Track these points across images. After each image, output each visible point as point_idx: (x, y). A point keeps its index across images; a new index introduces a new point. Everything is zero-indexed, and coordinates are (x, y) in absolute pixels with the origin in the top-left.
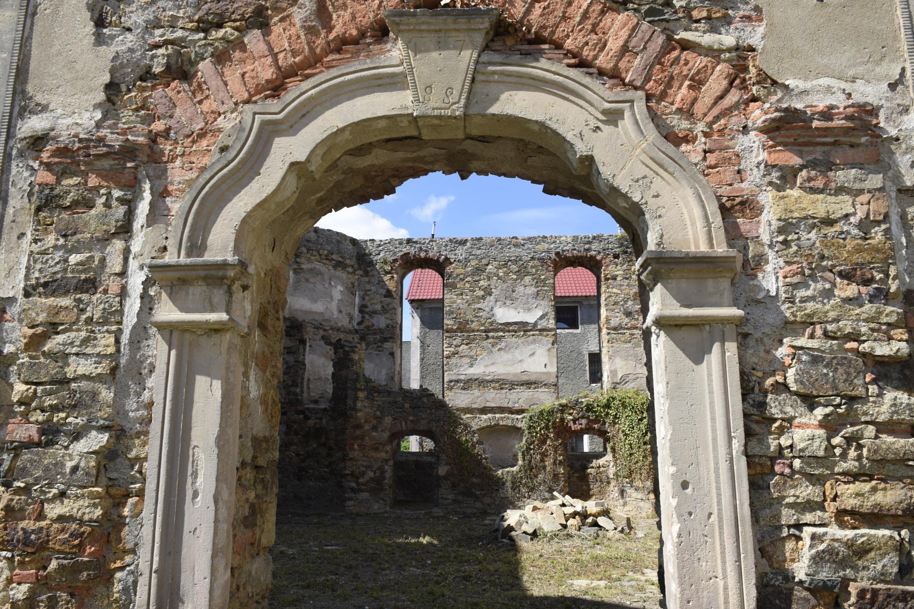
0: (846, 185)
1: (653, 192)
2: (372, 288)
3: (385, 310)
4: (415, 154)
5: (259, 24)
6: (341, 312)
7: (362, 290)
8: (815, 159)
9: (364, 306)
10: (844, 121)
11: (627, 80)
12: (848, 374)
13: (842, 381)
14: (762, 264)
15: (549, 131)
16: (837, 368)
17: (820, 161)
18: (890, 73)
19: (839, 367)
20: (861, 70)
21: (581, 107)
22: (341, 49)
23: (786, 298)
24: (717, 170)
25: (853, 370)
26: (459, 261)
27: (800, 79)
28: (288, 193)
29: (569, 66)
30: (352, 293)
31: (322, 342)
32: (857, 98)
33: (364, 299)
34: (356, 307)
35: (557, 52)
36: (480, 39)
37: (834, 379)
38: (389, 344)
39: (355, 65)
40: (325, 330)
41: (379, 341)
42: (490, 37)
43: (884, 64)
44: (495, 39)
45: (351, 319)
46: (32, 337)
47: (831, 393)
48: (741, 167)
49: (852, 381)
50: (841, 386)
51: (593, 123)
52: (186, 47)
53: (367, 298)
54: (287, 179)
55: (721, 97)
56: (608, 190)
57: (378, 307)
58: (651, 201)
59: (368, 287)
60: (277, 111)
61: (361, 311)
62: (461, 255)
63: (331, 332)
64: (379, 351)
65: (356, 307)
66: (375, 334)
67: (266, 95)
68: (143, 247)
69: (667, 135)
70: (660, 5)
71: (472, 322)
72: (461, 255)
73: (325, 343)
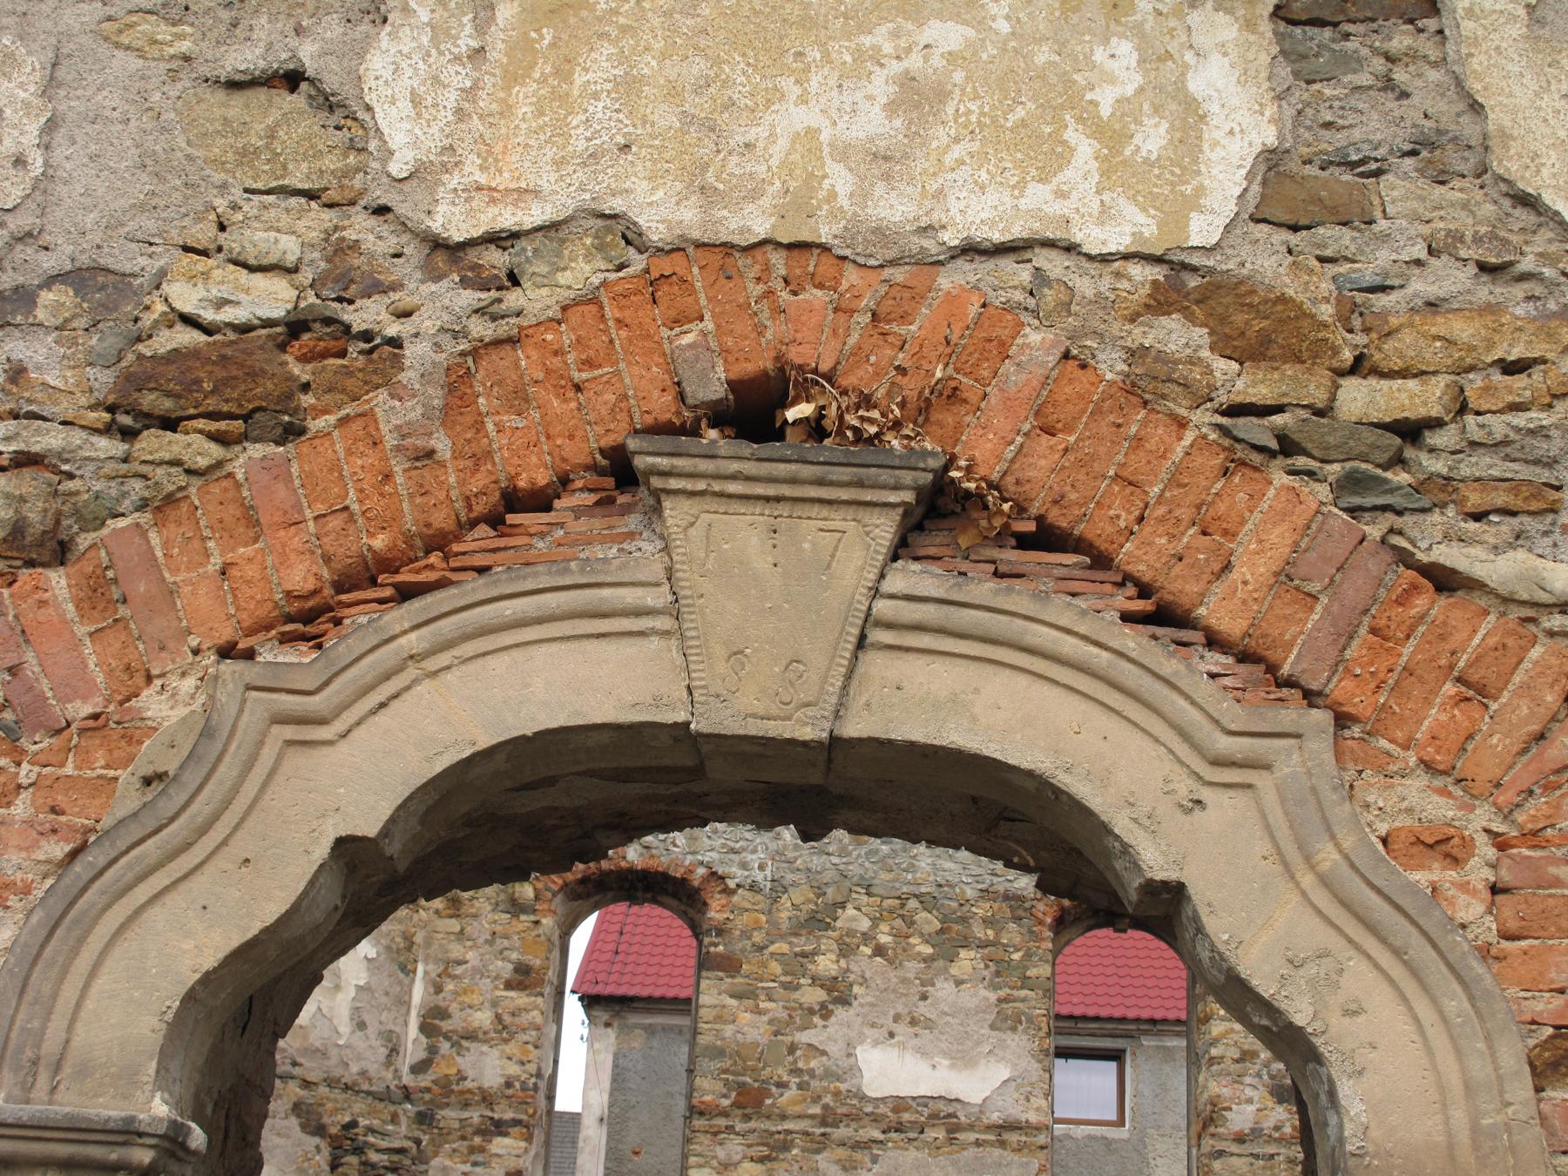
2: (470, 955)
3: (503, 1029)
4: (676, 789)
5: (280, 430)
6: (361, 1025)
7: (437, 961)
9: (443, 1014)
11: (1286, 670)
15: (1064, 798)
21: (396, 696)
22: (503, 522)
24: (1523, 943)
26: (753, 887)
28: (318, 915)
29: (1127, 617)
30: (403, 968)
31: (294, 1122)
33: (439, 989)
34: (414, 1013)
35: (1099, 575)
36: (885, 528)
38: (507, 1141)
39: (536, 574)
40: (307, 1084)
41: (479, 1132)
42: (914, 520)
44: (927, 523)
45: (394, 1051)
51: (1184, 787)
52: (71, 476)
53: (450, 986)
54: (321, 880)
56: (1222, 978)
57: (483, 1018)
58: (1337, 1022)
59: (456, 951)
60: (311, 688)
61: (427, 1029)
62: (762, 867)
63: (323, 1090)
64: (475, 1164)
65: (414, 1013)
66: (466, 1105)
67: (283, 634)
69: (1388, 835)
70: (1378, 466)
71: (782, 1085)
72: (762, 867)
73: (304, 1127)
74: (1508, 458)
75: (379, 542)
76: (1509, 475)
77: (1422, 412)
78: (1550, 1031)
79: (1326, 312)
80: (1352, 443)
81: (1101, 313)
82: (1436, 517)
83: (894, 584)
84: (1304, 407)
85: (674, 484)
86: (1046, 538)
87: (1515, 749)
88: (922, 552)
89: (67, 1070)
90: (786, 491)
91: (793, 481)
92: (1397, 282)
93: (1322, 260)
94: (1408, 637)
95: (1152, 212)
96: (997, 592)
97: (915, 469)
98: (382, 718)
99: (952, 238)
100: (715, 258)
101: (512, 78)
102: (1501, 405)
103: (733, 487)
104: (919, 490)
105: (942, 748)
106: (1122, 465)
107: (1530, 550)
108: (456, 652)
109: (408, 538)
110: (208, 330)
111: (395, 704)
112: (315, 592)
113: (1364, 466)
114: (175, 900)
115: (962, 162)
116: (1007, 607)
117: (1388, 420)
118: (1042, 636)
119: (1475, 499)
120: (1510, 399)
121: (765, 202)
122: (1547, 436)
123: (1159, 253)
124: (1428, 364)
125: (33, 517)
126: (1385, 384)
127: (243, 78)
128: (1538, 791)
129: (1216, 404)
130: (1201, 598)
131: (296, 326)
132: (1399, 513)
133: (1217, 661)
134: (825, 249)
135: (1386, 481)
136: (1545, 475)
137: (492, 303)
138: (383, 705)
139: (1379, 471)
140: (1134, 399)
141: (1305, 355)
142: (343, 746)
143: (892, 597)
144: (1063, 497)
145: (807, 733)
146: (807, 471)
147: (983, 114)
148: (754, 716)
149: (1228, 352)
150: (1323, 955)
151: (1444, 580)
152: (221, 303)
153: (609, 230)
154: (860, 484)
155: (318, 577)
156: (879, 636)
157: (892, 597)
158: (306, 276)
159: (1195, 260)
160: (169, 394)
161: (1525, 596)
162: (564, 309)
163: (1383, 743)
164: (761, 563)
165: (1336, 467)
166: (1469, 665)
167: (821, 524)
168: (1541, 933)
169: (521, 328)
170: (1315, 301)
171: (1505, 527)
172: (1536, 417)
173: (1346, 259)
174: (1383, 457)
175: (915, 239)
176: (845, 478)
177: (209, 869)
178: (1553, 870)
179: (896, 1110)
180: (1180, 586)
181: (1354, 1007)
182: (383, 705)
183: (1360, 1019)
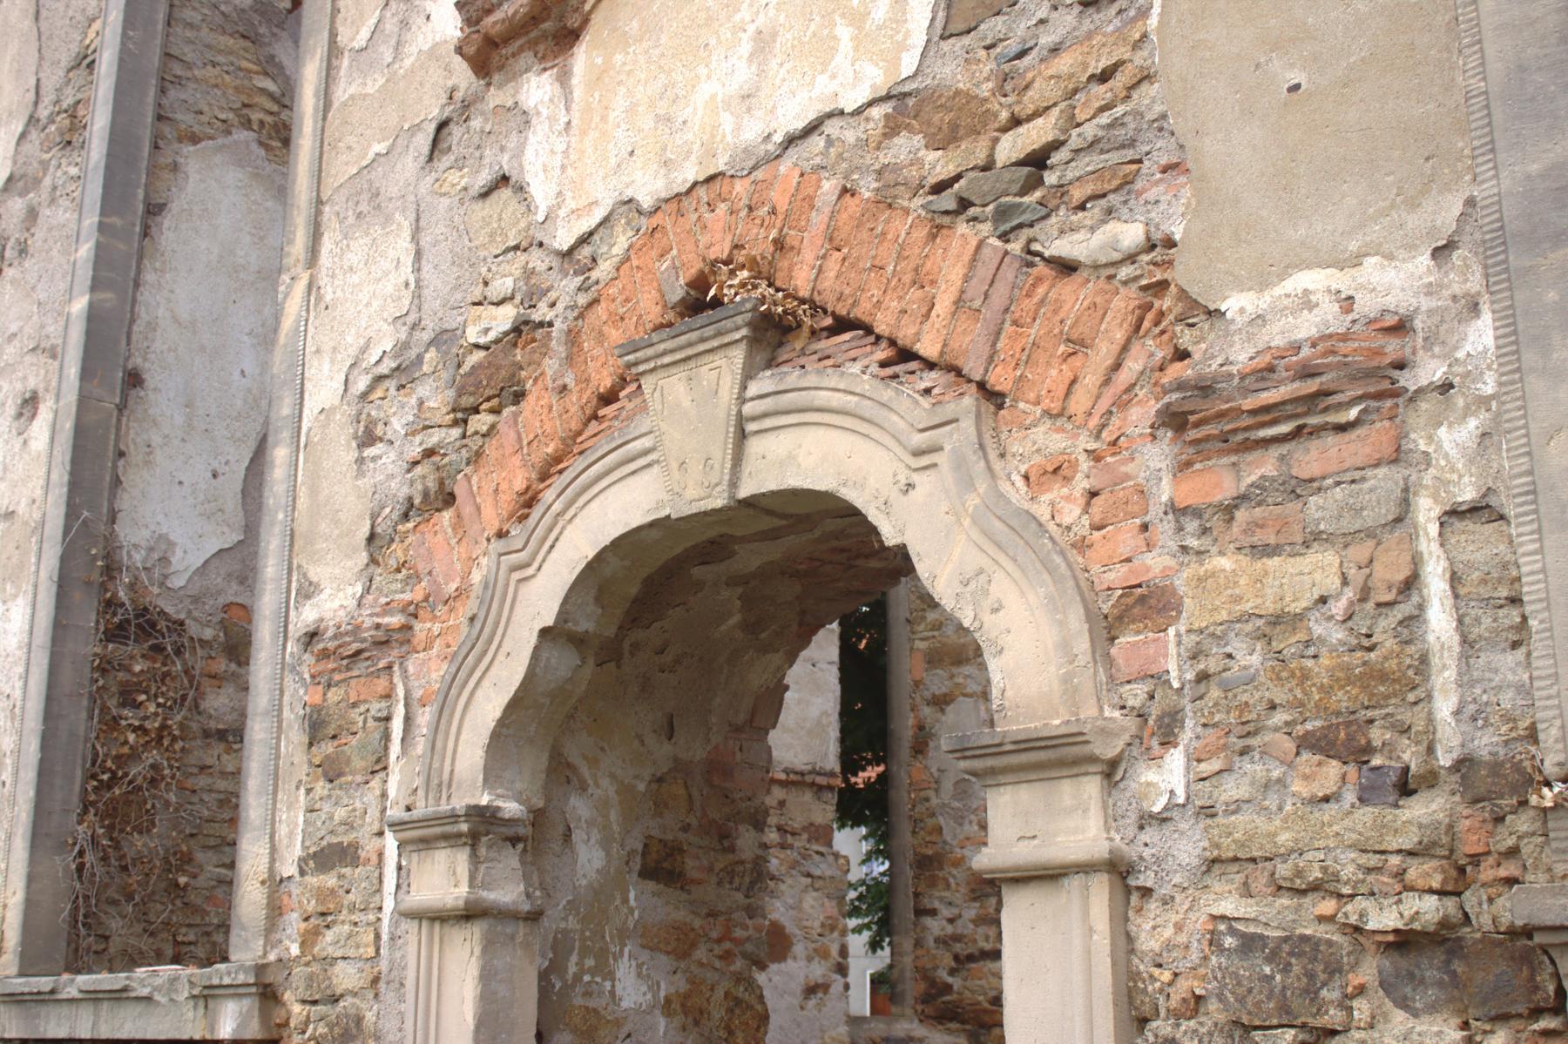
0: (1322, 527)
1: (987, 604)
8: (1262, 477)
10: (1296, 385)
12: (1311, 976)
13: (1297, 992)
14: (1176, 731)
16: (1290, 964)
17: (1273, 480)
18: (1439, 223)
19: (1293, 961)
20: (1375, 231)
21: (557, 539)
23: (1202, 808)
25: (1322, 967)
27: (1250, 289)
32: (1367, 305)
36: (738, 355)
37: (1284, 987)
43: (1428, 205)
44: (784, 340)
46: (307, 931)
47: (1275, 1022)
48: (1147, 519)
49: (1317, 993)
50: (1295, 1004)
55: (1117, 366)
58: (988, 619)
60: (520, 547)
68: (398, 790)
70: (1015, 195)
74: (1102, 152)
75: (550, 450)
76: (1100, 166)
77: (1044, 140)
78: (1120, 592)
79: (986, 89)
80: (998, 185)
81: (859, 152)
82: (1053, 219)
83: (751, 392)
84: (972, 169)
85: (641, 368)
86: (843, 325)
87: (1098, 383)
88: (780, 360)
89: (454, 786)
90: (690, 352)
91: (690, 345)
92: (1031, 43)
93: (988, 48)
94: (1034, 320)
95: (881, 64)
96: (800, 377)
97: (742, 313)
98: (554, 554)
99: (778, 138)
100: (673, 205)
101: (584, 133)
102: (1092, 112)
103: (667, 360)
104: (749, 324)
105: (785, 490)
106: (874, 257)
107: (1119, 219)
108: (577, 505)
109: (563, 440)
110: (486, 348)
111: (558, 544)
112: (528, 488)
113: (1008, 199)
114: (486, 683)
115: (784, 80)
116: (805, 385)
117: (1022, 156)
118: (822, 398)
119: (1077, 194)
120: (1097, 105)
121: (693, 158)
122: (1122, 124)
123: (884, 93)
124: (1049, 99)
125: (430, 485)
126: (1031, 125)
127: (486, 189)
128: (1114, 410)
129: (927, 189)
130: (917, 337)
131: (517, 330)
132: (1031, 226)
133: (930, 378)
134: (722, 174)
135: (1020, 205)
136: (1130, 154)
137: (584, 281)
138: (552, 547)
139: (1018, 200)
140: (881, 205)
141: (978, 128)
142: (540, 575)
143: (752, 399)
144: (842, 294)
145: (718, 503)
146: (694, 336)
147: (794, 39)
148: (695, 500)
149: (936, 146)
150: (981, 572)
151: (1066, 267)
152: (487, 331)
153: (630, 210)
154: (719, 334)
155: (528, 479)
156: (751, 427)
157: (752, 399)
158: (518, 300)
159: (907, 88)
160: (471, 394)
161: (1104, 261)
162: (618, 269)
163: (1022, 405)
164: (686, 403)
165: (991, 207)
166: (1071, 328)
167: (709, 366)
168: (1115, 520)
169: (599, 291)
170: (977, 85)
171: (1096, 210)
172: (1119, 110)
173: (1001, 40)
174: (1016, 188)
175: (762, 147)
176: (712, 333)
177: (496, 662)
178: (1123, 469)
179: (159, 613)
180: (905, 335)
181: (996, 606)
182: (552, 547)
183: (1001, 614)
